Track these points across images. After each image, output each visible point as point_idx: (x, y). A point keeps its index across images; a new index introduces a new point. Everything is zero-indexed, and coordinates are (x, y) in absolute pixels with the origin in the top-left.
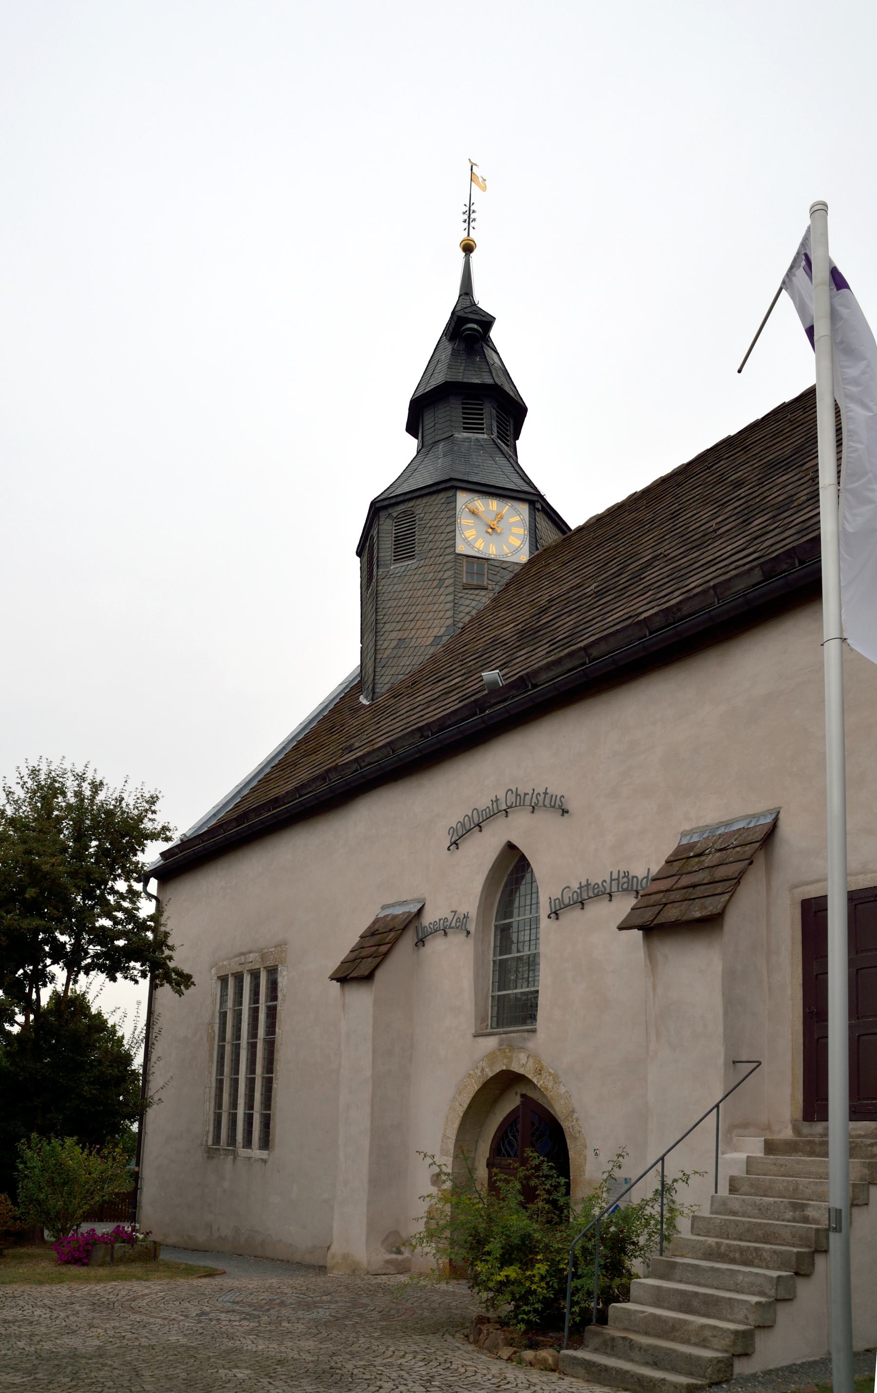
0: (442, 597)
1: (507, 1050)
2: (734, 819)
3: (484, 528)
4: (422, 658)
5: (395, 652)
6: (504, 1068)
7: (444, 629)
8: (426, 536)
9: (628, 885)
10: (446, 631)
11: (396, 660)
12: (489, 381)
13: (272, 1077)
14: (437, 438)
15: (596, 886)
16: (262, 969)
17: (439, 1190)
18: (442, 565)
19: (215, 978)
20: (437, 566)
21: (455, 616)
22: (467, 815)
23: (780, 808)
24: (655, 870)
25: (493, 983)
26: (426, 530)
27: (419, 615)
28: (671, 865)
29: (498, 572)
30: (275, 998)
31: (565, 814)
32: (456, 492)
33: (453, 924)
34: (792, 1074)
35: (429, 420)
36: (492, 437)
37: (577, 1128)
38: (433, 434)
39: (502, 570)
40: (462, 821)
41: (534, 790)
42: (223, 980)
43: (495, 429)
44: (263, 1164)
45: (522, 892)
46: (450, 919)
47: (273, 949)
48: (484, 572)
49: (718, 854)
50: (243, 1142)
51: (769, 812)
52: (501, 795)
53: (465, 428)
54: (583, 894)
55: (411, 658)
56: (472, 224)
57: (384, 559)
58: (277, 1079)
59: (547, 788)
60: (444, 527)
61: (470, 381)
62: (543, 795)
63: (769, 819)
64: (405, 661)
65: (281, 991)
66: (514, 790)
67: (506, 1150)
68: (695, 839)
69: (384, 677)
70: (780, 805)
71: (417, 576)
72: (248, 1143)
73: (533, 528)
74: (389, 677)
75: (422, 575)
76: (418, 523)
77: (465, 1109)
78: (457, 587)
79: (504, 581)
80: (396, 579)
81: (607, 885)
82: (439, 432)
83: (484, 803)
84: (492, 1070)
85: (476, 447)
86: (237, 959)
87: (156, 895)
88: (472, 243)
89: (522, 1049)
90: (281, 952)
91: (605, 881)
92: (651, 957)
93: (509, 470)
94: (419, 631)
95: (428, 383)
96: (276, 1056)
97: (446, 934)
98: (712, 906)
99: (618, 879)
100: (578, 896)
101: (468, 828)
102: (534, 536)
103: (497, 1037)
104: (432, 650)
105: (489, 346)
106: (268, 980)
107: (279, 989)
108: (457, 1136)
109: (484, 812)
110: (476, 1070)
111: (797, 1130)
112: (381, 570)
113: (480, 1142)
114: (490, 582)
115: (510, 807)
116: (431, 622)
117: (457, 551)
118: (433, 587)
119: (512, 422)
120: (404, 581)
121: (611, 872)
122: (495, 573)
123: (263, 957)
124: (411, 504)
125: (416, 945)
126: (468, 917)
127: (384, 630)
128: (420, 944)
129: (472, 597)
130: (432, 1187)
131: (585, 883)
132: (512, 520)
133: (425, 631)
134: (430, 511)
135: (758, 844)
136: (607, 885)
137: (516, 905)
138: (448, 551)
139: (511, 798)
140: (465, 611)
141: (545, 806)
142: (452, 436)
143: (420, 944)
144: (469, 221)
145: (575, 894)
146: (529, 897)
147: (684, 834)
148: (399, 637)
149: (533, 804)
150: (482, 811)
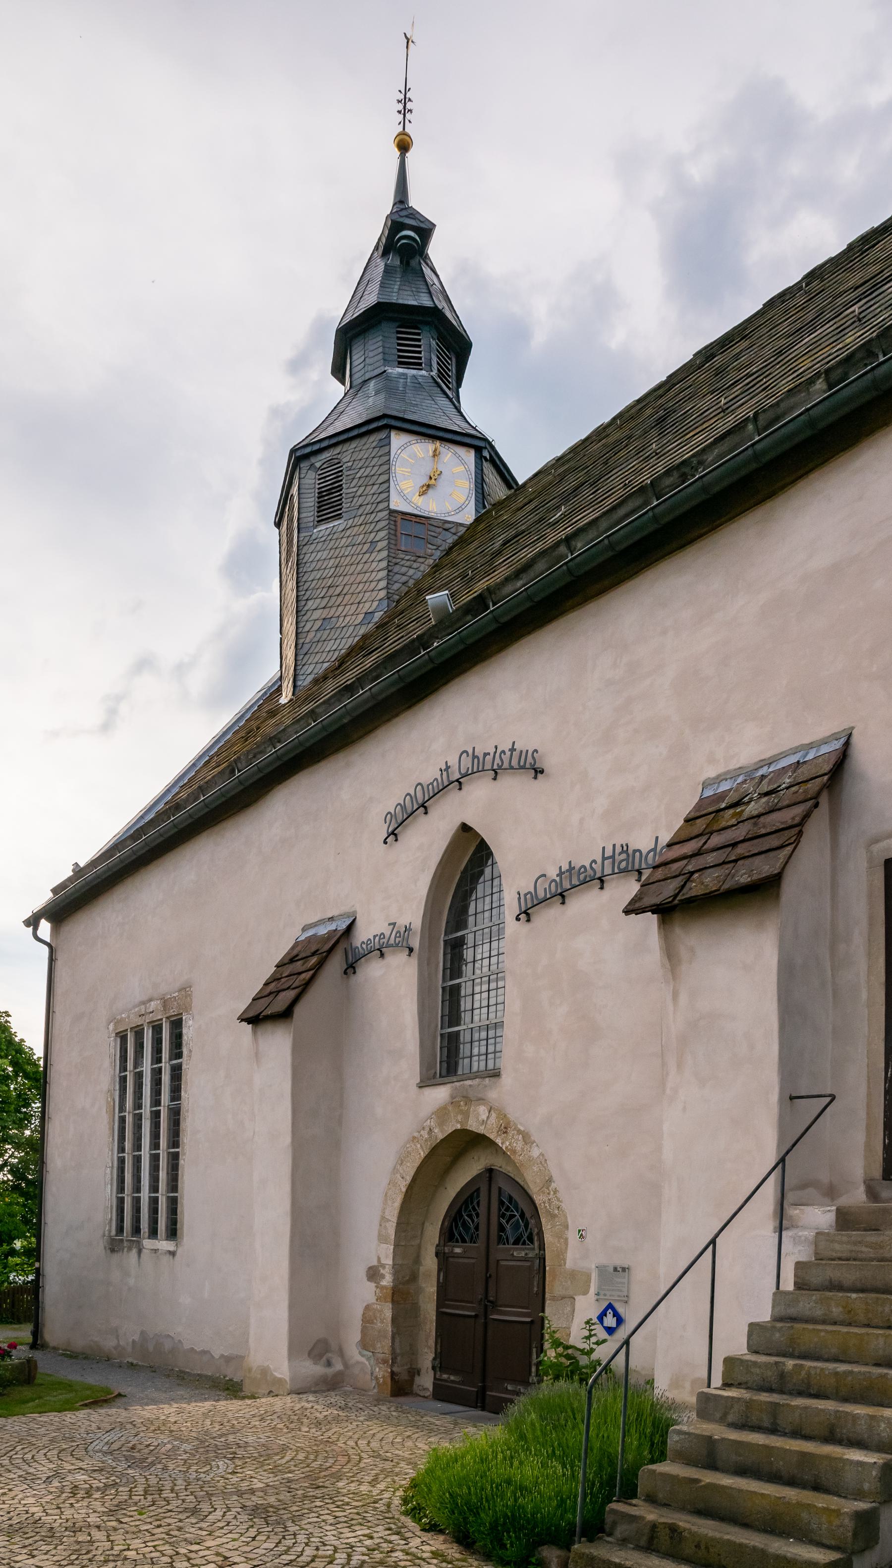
0: (375, 564)
1: (462, 1103)
2: (781, 753)
4: (350, 641)
5: (319, 635)
6: (459, 1127)
8: (355, 490)
9: (628, 864)
11: (320, 644)
12: (428, 303)
13: (178, 1152)
14: (367, 376)
15: (582, 870)
16: (164, 1020)
17: (377, 1287)
18: (373, 525)
19: (114, 1035)
20: (368, 526)
21: (390, 586)
22: (408, 794)
23: (853, 728)
24: (666, 837)
25: (442, 1017)
26: (355, 481)
27: (347, 588)
28: (691, 825)
29: (440, 534)
30: (179, 1055)
31: (539, 775)
32: (390, 432)
33: (392, 941)
34: (868, 1114)
35: (357, 357)
36: (432, 373)
37: (556, 1202)
38: (363, 371)
39: (444, 531)
40: (402, 803)
41: (496, 747)
42: (123, 1038)
43: (435, 366)
44: (171, 1257)
45: (480, 894)
46: (387, 934)
47: (177, 994)
49: (764, 800)
50: (149, 1232)
51: (835, 737)
52: (453, 761)
53: (400, 363)
54: (564, 882)
55: (338, 641)
56: (408, 116)
57: (305, 520)
58: (184, 1154)
59: (514, 743)
60: (376, 477)
61: (406, 302)
62: (508, 753)
63: (838, 745)
64: (330, 646)
65: (186, 1045)
66: (470, 752)
67: (460, 1235)
68: (725, 786)
69: (306, 667)
70: (852, 725)
71: (344, 540)
72: (153, 1233)
73: (480, 481)
74: (312, 666)
75: (350, 539)
77: (408, 1182)
78: (391, 551)
79: (446, 546)
80: (320, 544)
81: (597, 867)
82: (370, 368)
83: (430, 774)
84: (442, 1131)
85: (413, 385)
86: (137, 1009)
87: (48, 940)
88: (407, 138)
89: (481, 1100)
90: (186, 997)
91: (594, 861)
92: (670, 954)
93: (452, 411)
94: (348, 607)
95: (356, 307)
96: (183, 1125)
97: (382, 955)
98: (764, 867)
99: (613, 857)
100: (557, 886)
101: (409, 811)
102: (480, 491)
103: (449, 1086)
104: (363, 630)
105: (427, 264)
106: (171, 1034)
107: (184, 1043)
108: (399, 1218)
109: (430, 787)
110: (422, 1132)
111: (872, 1194)
112: (302, 535)
113: (427, 1224)
115: (466, 775)
116: (361, 595)
117: (392, 507)
118: (363, 551)
119: (454, 360)
120: (329, 547)
121: (604, 848)
123: (165, 1003)
124: (338, 450)
125: (345, 973)
126: (410, 929)
127: (306, 608)
128: (350, 971)
130: (369, 1283)
131: (567, 867)
133: (354, 607)
134: (359, 457)
135: (826, 778)
136: (597, 867)
137: (471, 910)
138: (381, 506)
139: (467, 762)
141: (512, 768)
143: (350, 971)
144: (405, 112)
145: (553, 884)
146: (488, 899)
147: (705, 785)
148: (323, 616)
149: (495, 767)
150: (428, 785)
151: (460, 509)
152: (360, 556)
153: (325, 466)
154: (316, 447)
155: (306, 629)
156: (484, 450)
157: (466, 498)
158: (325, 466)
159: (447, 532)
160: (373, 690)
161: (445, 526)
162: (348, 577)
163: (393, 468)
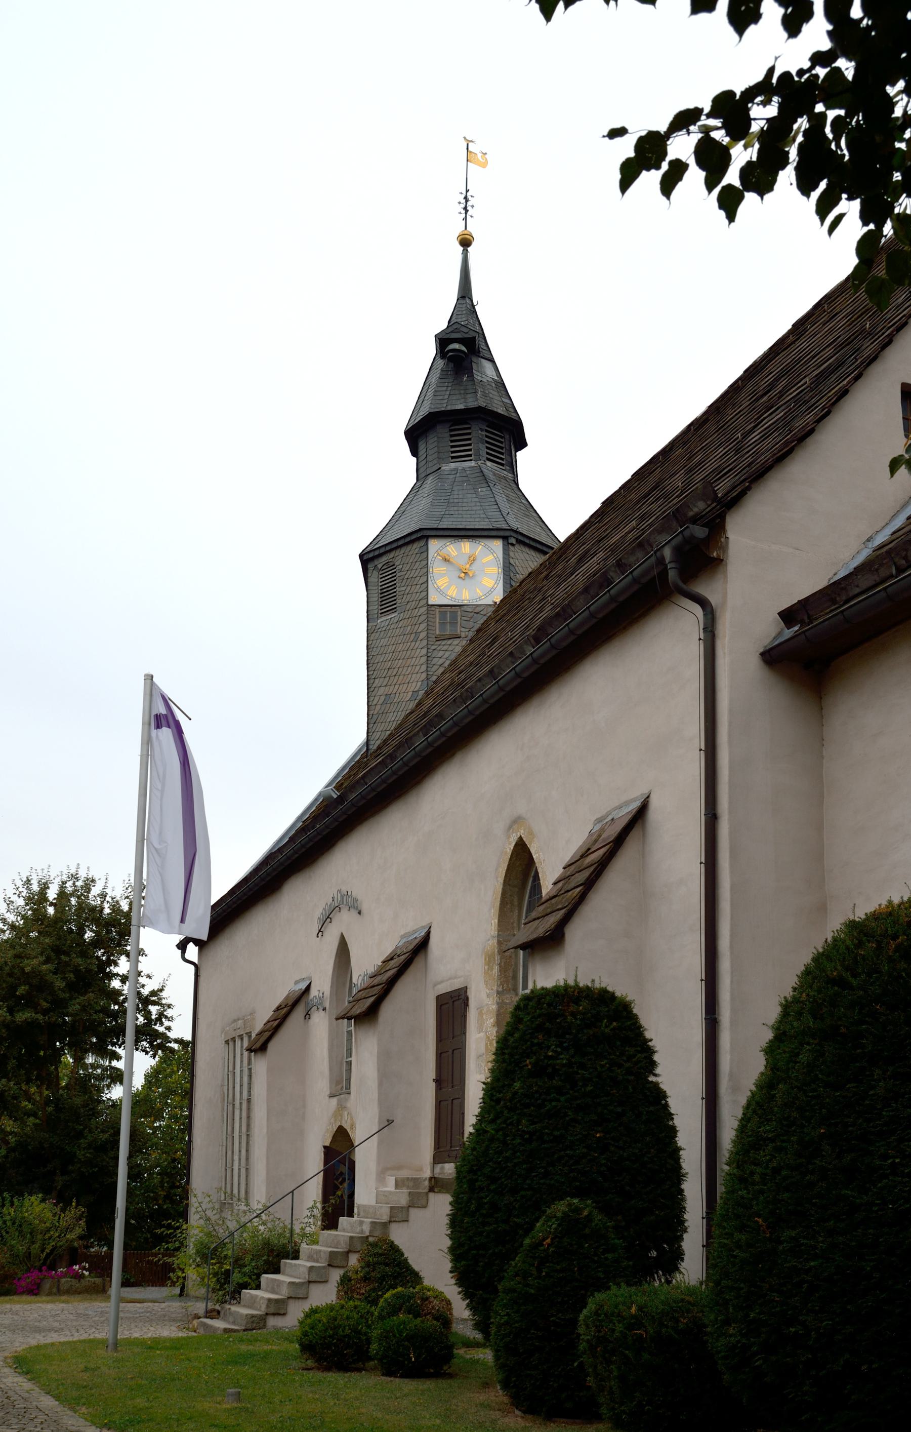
3: (457, 573)
7: (419, 684)
10: (421, 685)
14: (429, 471)
27: (401, 670)
29: (471, 618)
32: (427, 541)
42: (227, 1042)
48: (457, 620)
53: (453, 458)
60: (418, 578)
61: (453, 408)
64: (391, 717)
69: (375, 734)
75: (402, 629)
76: (399, 574)
80: (383, 633)
114: (463, 630)
117: (430, 603)
120: (388, 636)
122: (468, 619)
124: (392, 555)
127: (374, 685)
129: (445, 648)
132: (485, 560)
140: (438, 663)
142: (440, 468)
148: (385, 693)
151: (490, 593)
152: (409, 644)
153: (384, 567)
154: (377, 553)
155: (375, 703)
156: (509, 538)
157: (494, 582)
158: (384, 567)
159: (478, 615)
160: (302, 842)
161: (473, 610)
162: (401, 661)
163: (431, 570)
